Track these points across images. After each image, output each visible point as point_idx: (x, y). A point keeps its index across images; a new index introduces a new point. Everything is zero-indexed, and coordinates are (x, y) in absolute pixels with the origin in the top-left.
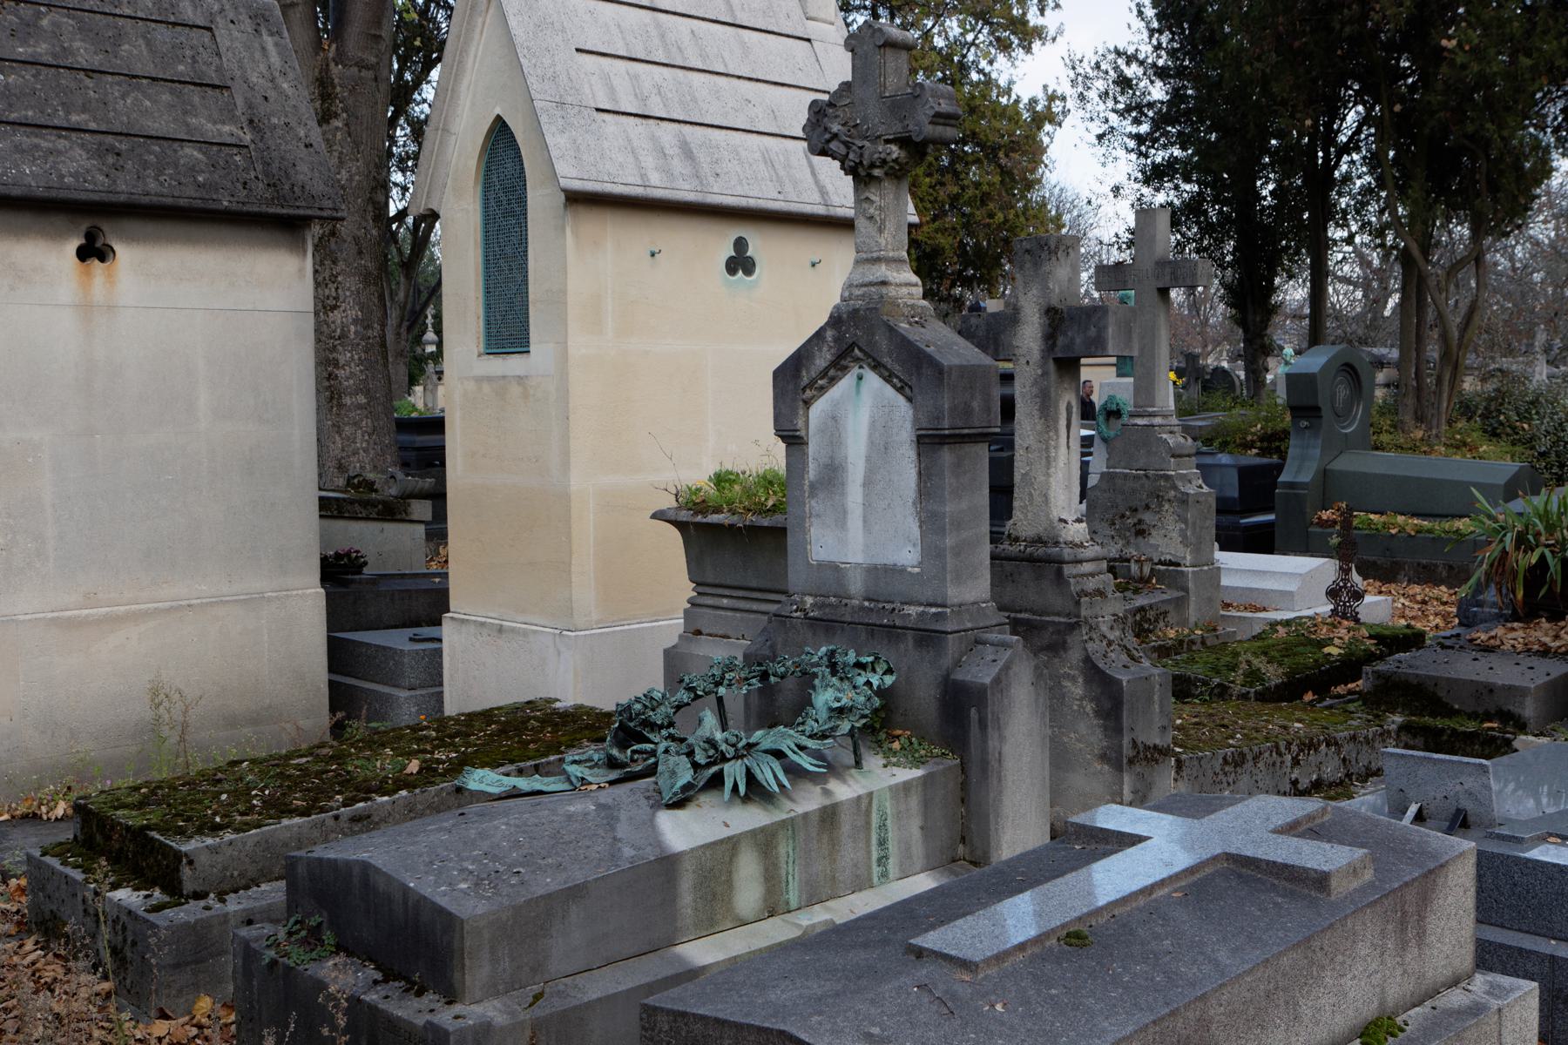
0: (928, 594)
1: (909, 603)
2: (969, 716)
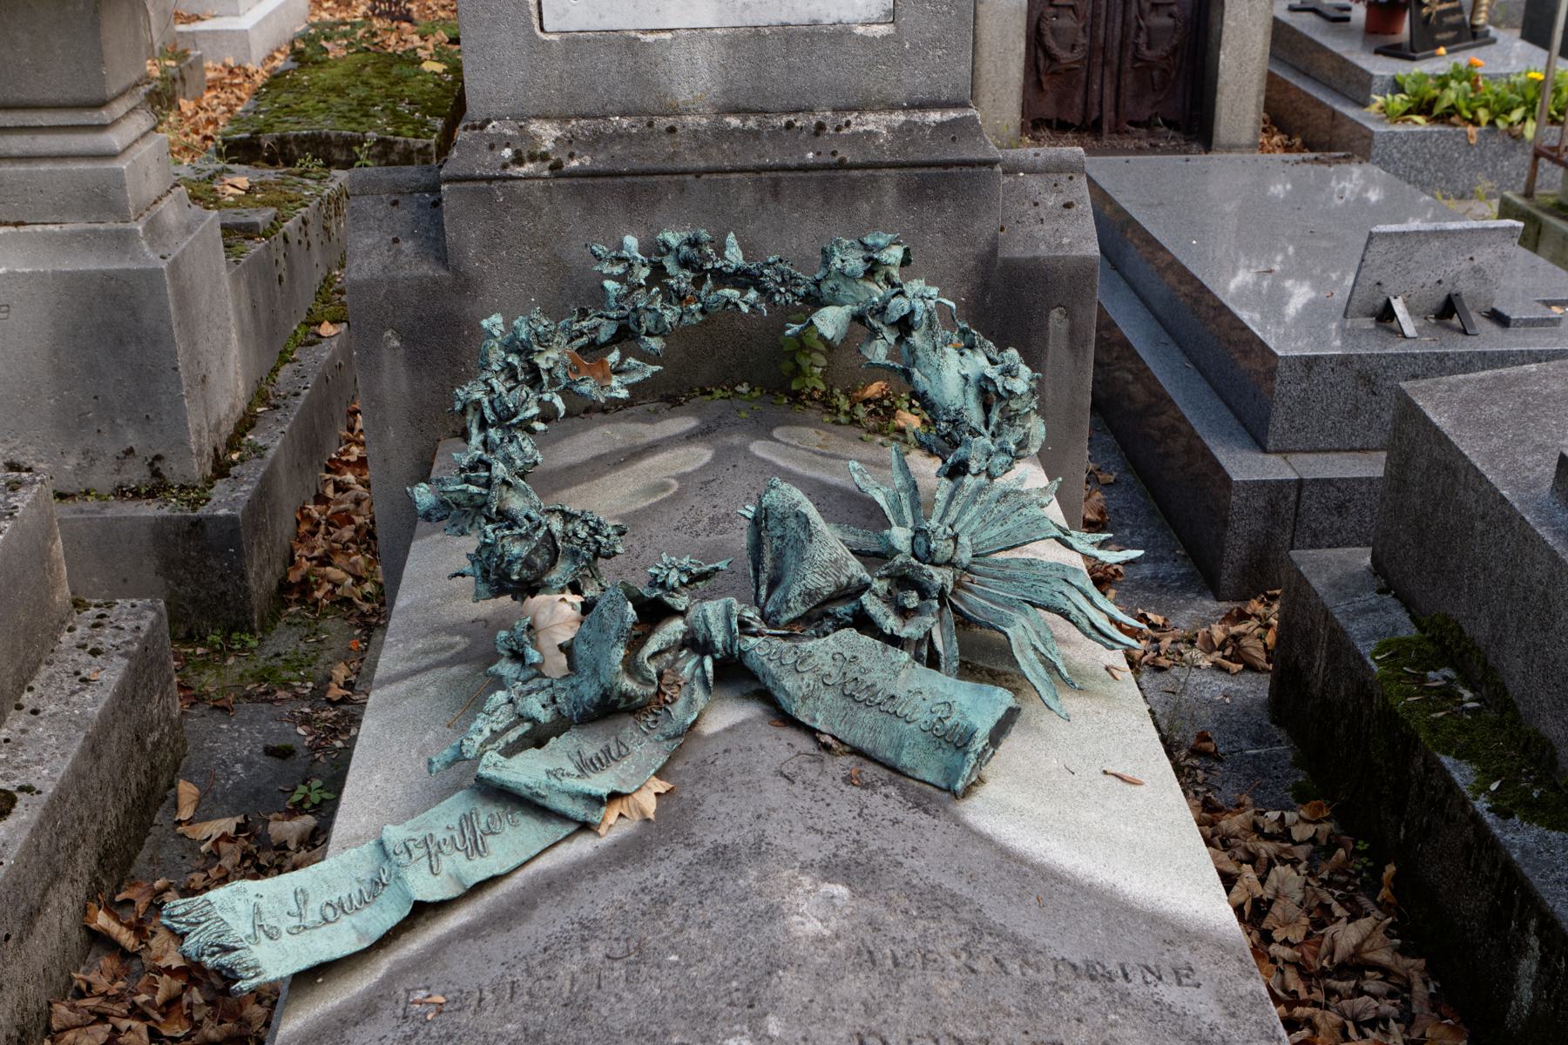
0: (918, 82)
1: (861, 109)
2: (1044, 327)
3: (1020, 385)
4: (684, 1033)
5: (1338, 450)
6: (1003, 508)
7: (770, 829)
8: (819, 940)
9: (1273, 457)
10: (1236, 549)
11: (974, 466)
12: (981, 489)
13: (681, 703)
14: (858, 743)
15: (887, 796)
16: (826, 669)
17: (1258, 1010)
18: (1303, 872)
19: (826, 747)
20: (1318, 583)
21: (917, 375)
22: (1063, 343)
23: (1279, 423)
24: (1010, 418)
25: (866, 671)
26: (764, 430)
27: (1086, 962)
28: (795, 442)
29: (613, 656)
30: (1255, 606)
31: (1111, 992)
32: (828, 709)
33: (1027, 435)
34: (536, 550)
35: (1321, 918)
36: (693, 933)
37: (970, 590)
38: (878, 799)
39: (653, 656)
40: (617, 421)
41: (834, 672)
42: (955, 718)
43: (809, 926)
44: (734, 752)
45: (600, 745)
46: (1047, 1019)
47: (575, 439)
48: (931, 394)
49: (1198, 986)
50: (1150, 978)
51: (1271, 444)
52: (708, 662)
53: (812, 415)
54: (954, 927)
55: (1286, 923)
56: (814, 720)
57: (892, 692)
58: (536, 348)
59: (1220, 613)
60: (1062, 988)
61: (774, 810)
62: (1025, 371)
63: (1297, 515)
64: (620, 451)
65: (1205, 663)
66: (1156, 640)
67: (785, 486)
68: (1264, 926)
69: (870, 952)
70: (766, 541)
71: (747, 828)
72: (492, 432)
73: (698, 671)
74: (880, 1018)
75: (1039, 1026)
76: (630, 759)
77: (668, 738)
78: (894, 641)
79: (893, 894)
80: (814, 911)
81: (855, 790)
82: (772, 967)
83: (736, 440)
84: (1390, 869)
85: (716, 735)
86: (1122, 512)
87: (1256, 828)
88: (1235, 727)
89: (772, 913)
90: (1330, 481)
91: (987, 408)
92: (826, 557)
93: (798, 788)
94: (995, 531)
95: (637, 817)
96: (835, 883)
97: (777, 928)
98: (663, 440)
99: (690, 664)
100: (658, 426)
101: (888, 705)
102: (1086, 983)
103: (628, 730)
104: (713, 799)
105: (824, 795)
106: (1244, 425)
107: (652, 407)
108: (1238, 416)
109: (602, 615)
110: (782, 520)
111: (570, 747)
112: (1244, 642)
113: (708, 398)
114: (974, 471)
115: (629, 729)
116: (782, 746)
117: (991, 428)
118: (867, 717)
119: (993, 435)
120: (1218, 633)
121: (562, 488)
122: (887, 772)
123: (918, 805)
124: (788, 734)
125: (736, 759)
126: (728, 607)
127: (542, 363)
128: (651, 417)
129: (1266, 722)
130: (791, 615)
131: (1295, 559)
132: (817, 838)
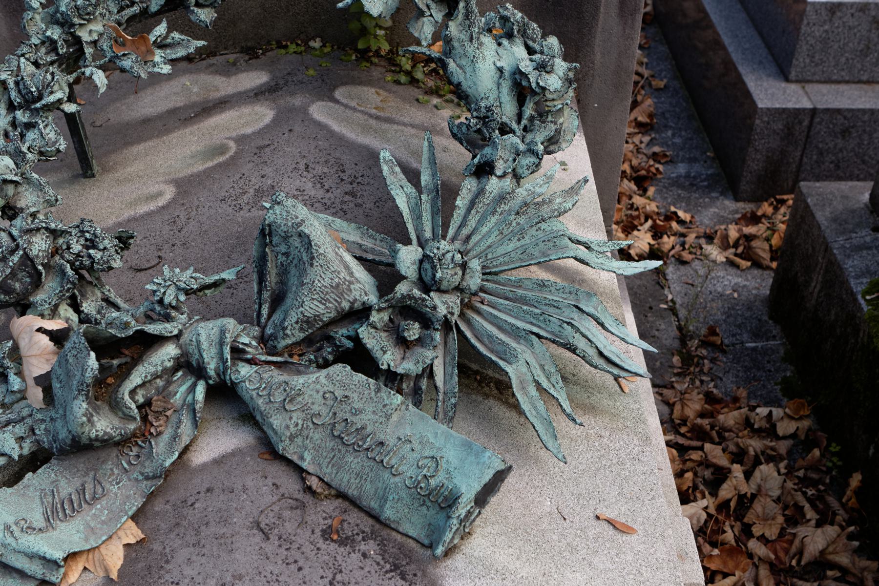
3: (553, 82)
5: (847, 82)
6: (522, 220)
9: (793, 86)
10: (755, 162)
11: (500, 167)
12: (502, 198)
13: (166, 437)
14: (343, 488)
16: (316, 408)
18: (783, 471)
19: (309, 490)
20: (822, 216)
21: (452, 66)
22: (614, 11)
23: (801, 59)
24: (542, 114)
25: (357, 412)
26: (325, 89)
28: (353, 104)
29: (76, 409)
30: (766, 208)
32: (317, 448)
33: (558, 132)
34: (13, 275)
35: (795, 518)
37: (478, 312)
38: (356, 557)
39: (133, 393)
40: (198, 71)
44: (217, 491)
45: (77, 482)
47: (158, 88)
48: (465, 85)
51: (793, 75)
52: (201, 389)
53: (376, 72)
55: (766, 519)
56: (302, 458)
57: (382, 437)
58: (76, 20)
59: (737, 212)
62: (561, 66)
63: (808, 136)
64: (193, 105)
65: (721, 258)
66: (684, 235)
67: (289, 202)
68: (746, 520)
70: (270, 256)
72: (19, 114)
73: (190, 398)
77: (147, 478)
78: (392, 379)
81: (333, 546)
83: (297, 101)
84: (856, 480)
85: (204, 467)
86: (667, 115)
87: (747, 423)
88: (740, 320)
90: (838, 111)
91: (521, 102)
92: (327, 282)
93: (270, 548)
94: (512, 246)
95: (102, 574)
98: (233, 96)
99: (183, 389)
100: (233, 79)
101: (375, 451)
103: (109, 465)
104: (183, 554)
105: (297, 555)
106: (773, 55)
107: (232, 58)
108: (768, 46)
109: (67, 360)
110: (286, 238)
111: (46, 485)
112: (755, 244)
113: (283, 51)
114: (499, 172)
115: (110, 465)
116: (264, 488)
117: (524, 122)
118: (354, 462)
119: (525, 129)
120: (733, 233)
121: (132, 144)
122: (371, 521)
123: (396, 567)
124: (277, 471)
126: (223, 332)
127: (84, 35)
128: (230, 69)
129: (765, 318)
130: (289, 342)
131: (805, 191)
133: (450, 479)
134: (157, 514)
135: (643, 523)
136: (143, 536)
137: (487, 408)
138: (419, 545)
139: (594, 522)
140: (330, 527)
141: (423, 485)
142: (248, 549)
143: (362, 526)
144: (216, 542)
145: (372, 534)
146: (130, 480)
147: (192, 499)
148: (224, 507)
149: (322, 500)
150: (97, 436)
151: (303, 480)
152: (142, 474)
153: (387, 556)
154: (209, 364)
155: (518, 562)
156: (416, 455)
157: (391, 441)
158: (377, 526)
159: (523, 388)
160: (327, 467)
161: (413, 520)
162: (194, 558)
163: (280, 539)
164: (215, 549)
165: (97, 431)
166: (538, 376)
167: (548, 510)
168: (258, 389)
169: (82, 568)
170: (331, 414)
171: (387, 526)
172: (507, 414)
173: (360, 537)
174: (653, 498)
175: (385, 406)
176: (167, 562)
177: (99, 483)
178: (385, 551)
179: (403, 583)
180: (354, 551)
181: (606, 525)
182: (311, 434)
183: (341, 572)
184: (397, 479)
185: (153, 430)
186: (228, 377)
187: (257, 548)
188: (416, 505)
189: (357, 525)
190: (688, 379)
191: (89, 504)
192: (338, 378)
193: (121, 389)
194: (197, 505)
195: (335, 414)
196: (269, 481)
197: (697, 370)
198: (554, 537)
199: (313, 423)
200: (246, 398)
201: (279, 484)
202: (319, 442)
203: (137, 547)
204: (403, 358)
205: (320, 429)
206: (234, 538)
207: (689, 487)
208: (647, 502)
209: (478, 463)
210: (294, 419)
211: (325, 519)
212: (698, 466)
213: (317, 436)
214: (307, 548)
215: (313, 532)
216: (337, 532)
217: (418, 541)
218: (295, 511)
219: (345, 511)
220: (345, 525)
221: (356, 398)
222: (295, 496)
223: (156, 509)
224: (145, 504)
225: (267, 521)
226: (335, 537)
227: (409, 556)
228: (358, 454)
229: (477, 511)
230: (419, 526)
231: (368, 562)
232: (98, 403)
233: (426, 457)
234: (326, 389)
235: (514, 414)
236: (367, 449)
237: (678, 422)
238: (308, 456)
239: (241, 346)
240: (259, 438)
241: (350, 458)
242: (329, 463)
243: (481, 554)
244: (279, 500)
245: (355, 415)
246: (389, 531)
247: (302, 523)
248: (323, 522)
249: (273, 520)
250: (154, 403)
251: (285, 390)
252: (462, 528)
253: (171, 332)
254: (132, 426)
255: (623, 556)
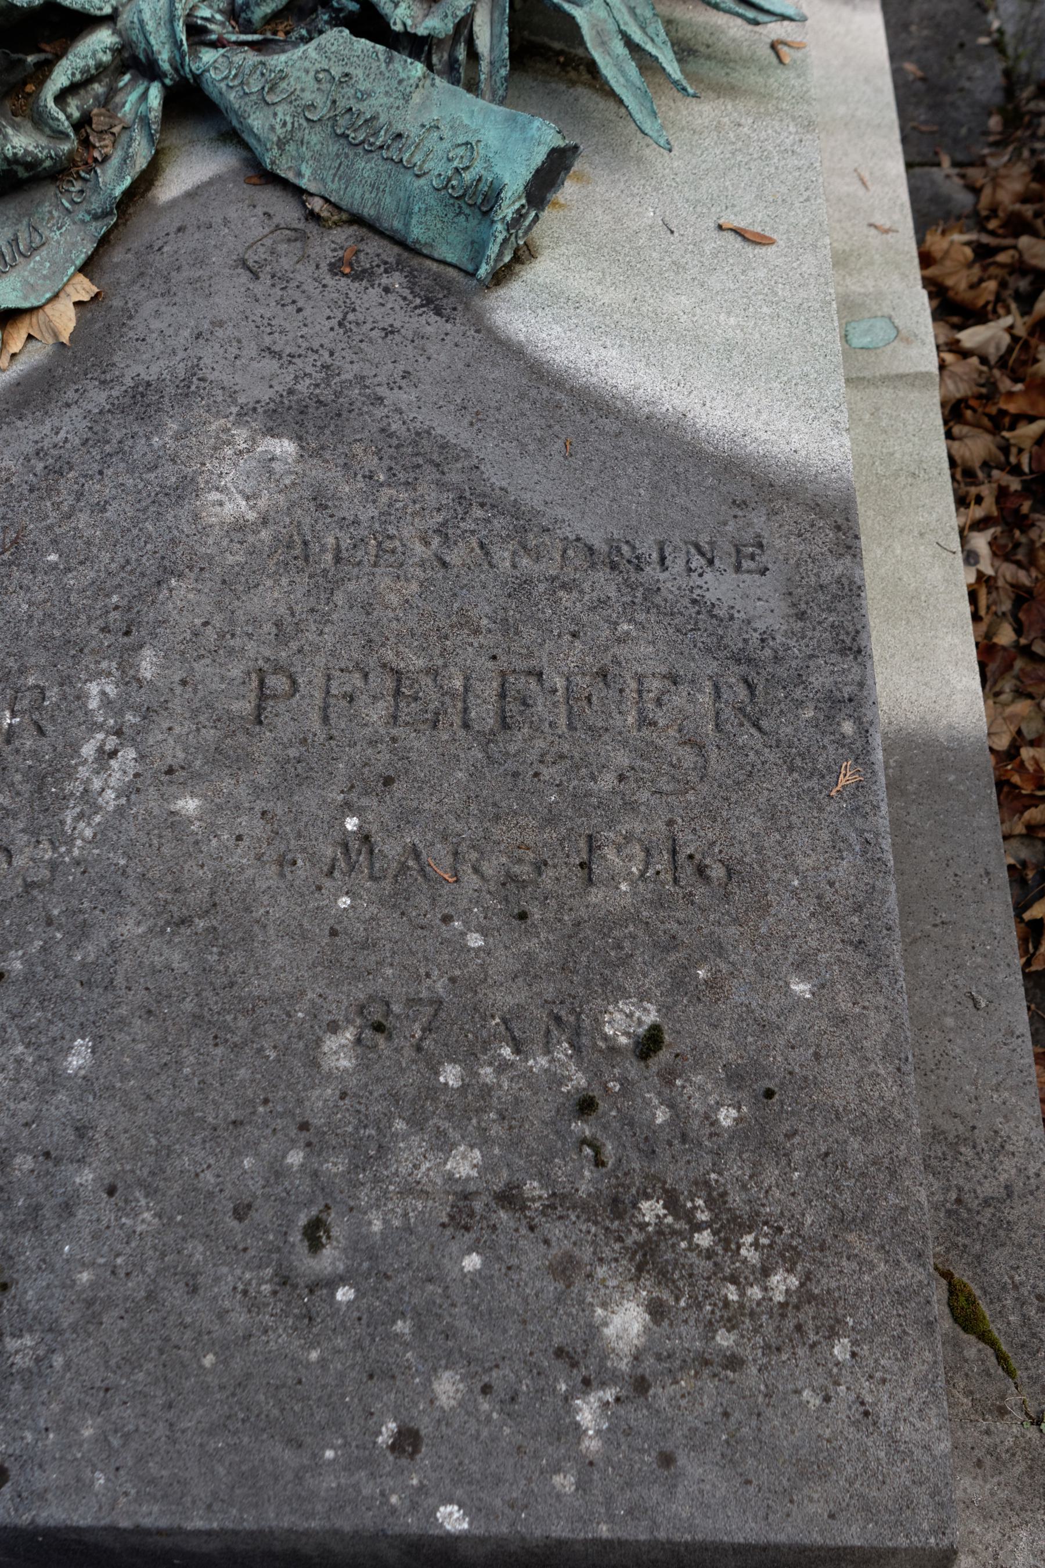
4: (43, 670)
7: (208, 354)
8: (239, 527)
13: (115, 161)
14: (356, 208)
15: (387, 290)
16: (308, 97)
17: (841, 606)
19: (313, 216)
25: (364, 96)
27: (610, 541)
31: (633, 587)
32: (317, 157)
36: (83, 519)
38: (374, 293)
39: (61, 98)
41: (319, 100)
42: (478, 169)
43: (229, 507)
44: (190, 229)
46: (530, 634)
49: (763, 571)
50: (697, 561)
54: (432, 497)
56: (299, 174)
57: (400, 127)
60: (564, 586)
61: (221, 324)
69: (305, 543)
71: (181, 354)
74: (294, 645)
75: (515, 647)
76: (44, 252)
77: (96, 217)
78: (417, 46)
79: (358, 449)
80: (241, 480)
81: (344, 282)
82: (168, 571)
85: (173, 203)
89: (185, 489)
93: (259, 289)
95: (51, 341)
96: (279, 436)
97: (184, 513)
99: (133, 97)
102: (601, 575)
103: (46, 207)
105: (297, 295)
115: (48, 204)
118: (366, 167)
122: (396, 250)
123: (428, 301)
125: (191, 241)
132: (270, 365)
133: (489, 168)
134: (117, 265)
135: (788, 231)
136: (96, 290)
137: (571, 99)
138: (462, 274)
139: (715, 234)
140: (341, 259)
141: (454, 183)
142: (231, 291)
143: (384, 257)
144: (190, 287)
145: (398, 264)
146: (75, 223)
147: (160, 243)
148: (199, 246)
149: (330, 228)
150: (15, 154)
151: (303, 204)
152: (88, 212)
153: (417, 289)
154: (160, 53)
155: (599, 287)
156: (446, 145)
157: (413, 130)
158: (406, 254)
159: (603, 43)
160: (333, 181)
161: (450, 238)
162: (163, 309)
163: (273, 277)
164: (189, 296)
165: (14, 147)
166: (626, 24)
167: (650, 222)
168: (226, 78)
169: (25, 336)
170: (329, 103)
171: (418, 253)
172: (601, 106)
173: (382, 269)
174: (808, 200)
175: (400, 82)
176: (130, 317)
177: (36, 230)
178: (414, 284)
179: (438, 318)
180: (372, 286)
181: (730, 236)
182: (306, 137)
183: (354, 310)
184: (422, 181)
185: (96, 154)
186: (187, 69)
187: (243, 289)
188: (451, 215)
189: (378, 255)
190: (1010, 148)
191: (25, 256)
192: (333, 49)
193: (42, 96)
194: (165, 249)
195: (334, 102)
196: (259, 211)
197: (1028, 133)
198: (654, 254)
199: (308, 120)
200: (215, 96)
201: (272, 212)
202: (318, 147)
203: (93, 306)
204: (426, 15)
205: (318, 128)
206: (212, 281)
207: (987, 303)
208: (797, 205)
209: (525, 140)
210: (280, 116)
211: (335, 250)
212: (1010, 274)
213: (314, 139)
214: (310, 286)
215: (318, 267)
216: (351, 265)
217: (460, 269)
218: (293, 244)
219: (362, 240)
220: (362, 256)
221: (361, 76)
222: (296, 225)
223: (115, 260)
224: (96, 251)
225: (256, 258)
226: (347, 270)
227: (448, 288)
228: (370, 156)
229: (533, 214)
230: (460, 247)
231: (391, 297)
232: (18, 119)
233: (459, 145)
234: (318, 66)
235: (612, 105)
236: (381, 147)
237: (984, 213)
238: (307, 171)
239: (199, 22)
240: (245, 160)
241: (360, 164)
242: (335, 175)
243: (548, 280)
244: (272, 232)
245: (362, 100)
246: (420, 260)
247: (304, 258)
248: (331, 254)
249: (263, 257)
250: (95, 120)
251: (263, 74)
252: (513, 239)
253: (101, 9)
254: (66, 147)
255: (751, 273)
